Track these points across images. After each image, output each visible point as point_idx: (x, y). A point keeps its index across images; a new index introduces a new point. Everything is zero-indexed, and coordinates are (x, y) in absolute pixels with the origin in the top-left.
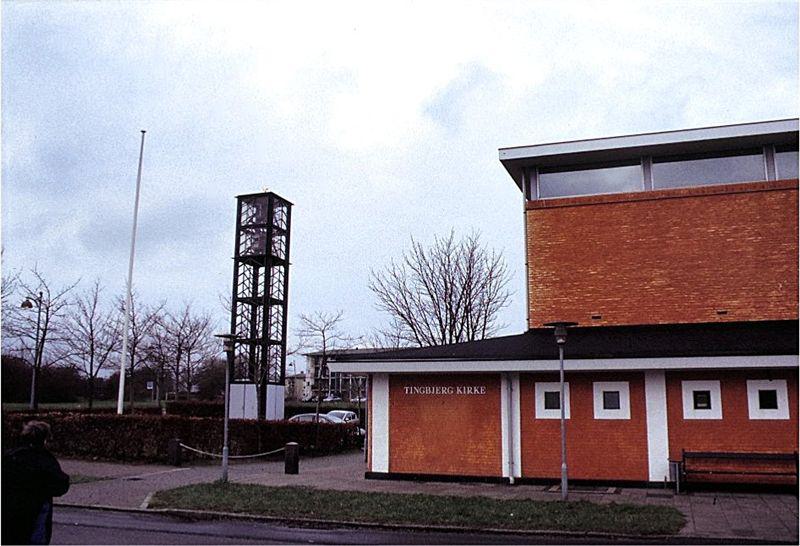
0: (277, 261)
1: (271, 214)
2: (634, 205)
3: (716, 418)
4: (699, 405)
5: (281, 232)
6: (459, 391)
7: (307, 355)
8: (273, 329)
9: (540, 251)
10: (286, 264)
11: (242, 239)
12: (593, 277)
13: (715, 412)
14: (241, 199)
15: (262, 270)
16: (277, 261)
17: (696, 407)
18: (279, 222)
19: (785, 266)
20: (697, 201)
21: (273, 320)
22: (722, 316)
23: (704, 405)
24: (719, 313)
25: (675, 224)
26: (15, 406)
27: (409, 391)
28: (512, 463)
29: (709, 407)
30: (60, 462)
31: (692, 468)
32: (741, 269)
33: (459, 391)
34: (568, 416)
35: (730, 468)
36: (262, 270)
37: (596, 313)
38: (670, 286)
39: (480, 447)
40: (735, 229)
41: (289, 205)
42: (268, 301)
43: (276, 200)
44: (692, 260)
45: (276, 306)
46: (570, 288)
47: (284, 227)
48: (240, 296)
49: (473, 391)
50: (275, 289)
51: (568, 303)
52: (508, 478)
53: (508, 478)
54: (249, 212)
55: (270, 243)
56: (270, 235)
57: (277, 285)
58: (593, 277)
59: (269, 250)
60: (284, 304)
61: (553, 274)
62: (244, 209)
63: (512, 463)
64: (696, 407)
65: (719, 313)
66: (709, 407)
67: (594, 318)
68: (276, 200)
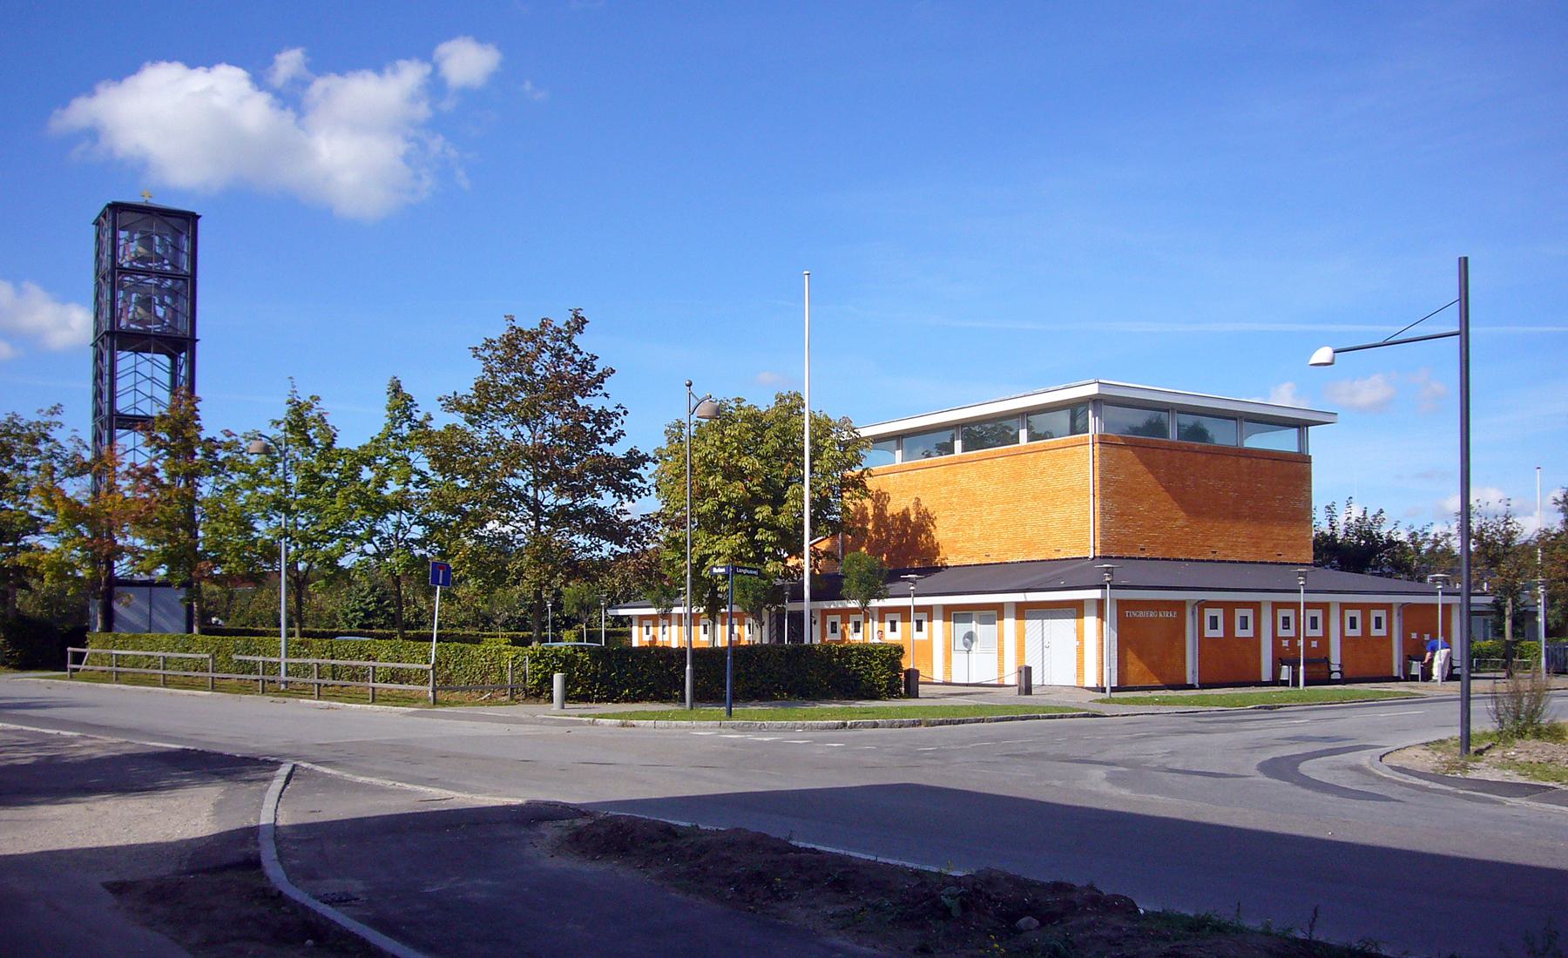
13: (1219, 633)
38: (1187, 527)
67: (1141, 549)
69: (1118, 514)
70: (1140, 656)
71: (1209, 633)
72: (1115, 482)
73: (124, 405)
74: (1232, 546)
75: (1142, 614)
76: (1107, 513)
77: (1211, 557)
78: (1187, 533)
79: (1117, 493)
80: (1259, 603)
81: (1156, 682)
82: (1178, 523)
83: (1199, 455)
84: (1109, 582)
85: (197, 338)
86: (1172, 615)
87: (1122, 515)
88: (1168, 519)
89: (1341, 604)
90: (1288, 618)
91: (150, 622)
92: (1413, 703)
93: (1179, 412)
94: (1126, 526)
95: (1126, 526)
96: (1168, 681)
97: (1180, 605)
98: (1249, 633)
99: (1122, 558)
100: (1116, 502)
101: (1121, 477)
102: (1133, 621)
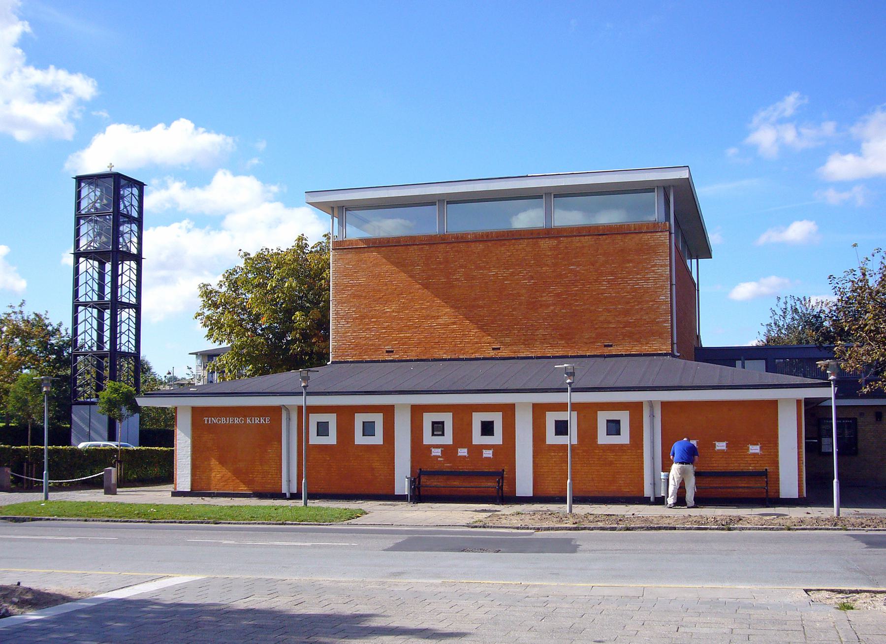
0: (128, 256)
1: (117, 198)
2: (427, 247)
3: (575, 443)
4: (435, 433)
5: (131, 219)
6: (248, 421)
7: (196, 354)
8: (124, 339)
9: (343, 289)
10: (138, 258)
11: (83, 230)
12: (388, 314)
13: (331, 439)
14: (80, 180)
15: (108, 267)
16: (128, 256)
17: (433, 435)
18: (129, 208)
19: (552, 308)
20: (481, 246)
21: (124, 327)
22: (495, 352)
23: (440, 433)
24: (494, 349)
25: (461, 267)
26: (172, 449)
27: (208, 421)
28: (289, 481)
29: (443, 434)
30: (136, 399)
31: (428, 483)
32: (514, 309)
33: (248, 421)
34: (575, 441)
35: (456, 483)
36: (108, 267)
37: (388, 348)
38: (454, 323)
39: (266, 468)
40: (513, 272)
41: (140, 186)
42: (116, 305)
43: (123, 182)
44: (475, 299)
45: (127, 310)
46: (367, 324)
47: (135, 214)
48: (82, 299)
49: (260, 421)
50: (125, 279)
51: (367, 338)
52: (285, 494)
53: (285, 494)
54: (91, 196)
55: (116, 234)
56: (116, 225)
57: (127, 273)
58: (388, 314)
59: (116, 242)
60: (137, 307)
61: (354, 311)
62: (84, 192)
63: (289, 481)
64: (433, 435)
65: (494, 349)
66: (443, 434)
67: (387, 352)
68: (123, 182)
69: (357, 318)
70: (222, 462)
71: (315, 440)
72: (353, 286)
73: (132, 312)
74: (525, 340)
75: (223, 420)
76: (342, 319)
77: (492, 354)
78: (453, 331)
79: (354, 296)
80: (392, 407)
81: (243, 489)
82: (440, 321)
83: (473, 245)
84: (570, 383)
85: (241, 263)
86: (265, 421)
87: (362, 317)
88: (427, 317)
89: (662, 403)
90: (443, 423)
91: (89, 437)
92: (69, 527)
93: (448, 203)
94: (367, 329)
95: (367, 329)
96: (259, 488)
97: (275, 412)
98: (378, 439)
99: (361, 362)
100: (354, 306)
101: (362, 280)
102: (212, 428)
